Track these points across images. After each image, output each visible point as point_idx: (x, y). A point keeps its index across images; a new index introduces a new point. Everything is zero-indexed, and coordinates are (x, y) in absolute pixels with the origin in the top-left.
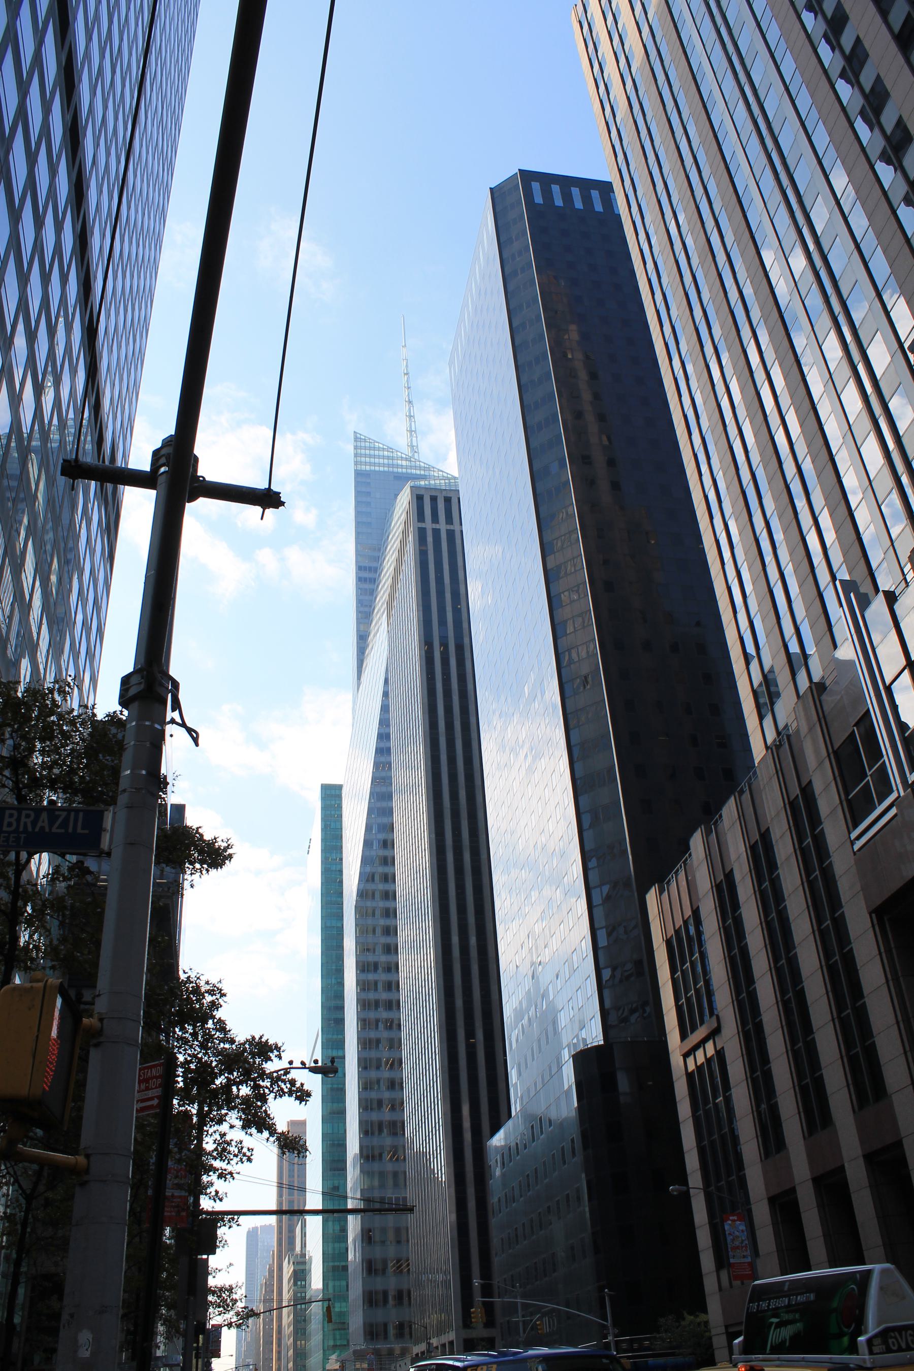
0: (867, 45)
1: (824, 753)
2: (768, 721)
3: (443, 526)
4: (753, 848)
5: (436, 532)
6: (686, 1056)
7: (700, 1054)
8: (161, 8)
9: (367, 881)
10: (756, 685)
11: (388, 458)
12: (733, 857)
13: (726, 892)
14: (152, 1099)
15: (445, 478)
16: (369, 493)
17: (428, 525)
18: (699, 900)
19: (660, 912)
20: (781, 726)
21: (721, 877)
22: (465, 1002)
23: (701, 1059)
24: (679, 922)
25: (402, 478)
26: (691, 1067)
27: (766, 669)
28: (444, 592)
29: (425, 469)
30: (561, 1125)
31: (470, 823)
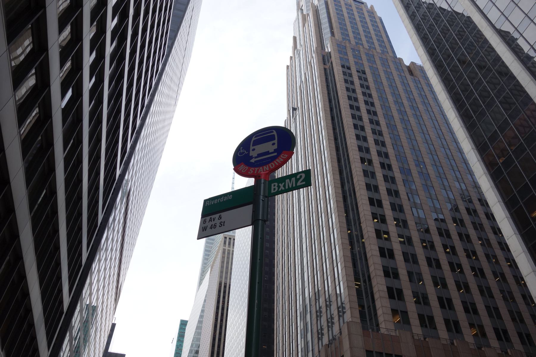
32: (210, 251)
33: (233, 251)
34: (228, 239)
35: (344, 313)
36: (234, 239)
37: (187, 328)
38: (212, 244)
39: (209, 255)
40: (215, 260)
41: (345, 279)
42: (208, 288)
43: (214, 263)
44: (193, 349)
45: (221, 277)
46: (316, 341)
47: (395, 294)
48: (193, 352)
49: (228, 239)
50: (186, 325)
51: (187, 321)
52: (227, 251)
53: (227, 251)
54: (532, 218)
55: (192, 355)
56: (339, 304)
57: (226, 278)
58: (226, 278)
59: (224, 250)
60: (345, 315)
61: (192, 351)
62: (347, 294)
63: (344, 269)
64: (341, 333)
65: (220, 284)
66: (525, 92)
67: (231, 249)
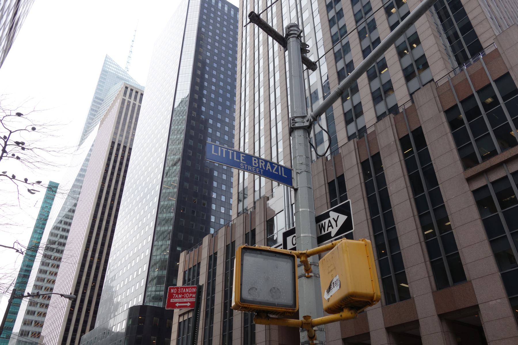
0: (351, 46)
1: (263, 220)
2: (241, 204)
3: (137, 103)
4: (227, 246)
5: (129, 102)
6: (180, 316)
7: (186, 317)
8: (190, 2)
9: (58, 223)
10: (240, 191)
11: (117, 69)
12: (219, 247)
13: (213, 259)
14: (187, 302)
15: (136, 84)
16: (105, 79)
17: (127, 98)
18: (201, 260)
19: (184, 261)
20: (245, 207)
21: (212, 253)
22: (86, 278)
23: (186, 317)
24: (191, 266)
25: (122, 79)
26: (181, 320)
27: (245, 187)
28: (125, 125)
29: (129, 78)
30: (118, 334)
31: (103, 209)
32: (96, 111)
33: (139, 107)
34: (129, 90)
35: (244, 198)
36: (142, 95)
38: (100, 104)
39: (95, 115)
40: (109, 111)
43: (106, 116)
44: (66, 206)
45: (115, 133)
48: (67, 210)
49: (129, 90)
52: (131, 104)
53: (131, 104)
54: (433, 229)
55: (65, 213)
56: (241, 189)
58: (127, 138)
59: (123, 101)
60: (245, 201)
61: (65, 209)
62: (418, 111)
64: (254, 207)
66: (461, 261)
67: (137, 103)
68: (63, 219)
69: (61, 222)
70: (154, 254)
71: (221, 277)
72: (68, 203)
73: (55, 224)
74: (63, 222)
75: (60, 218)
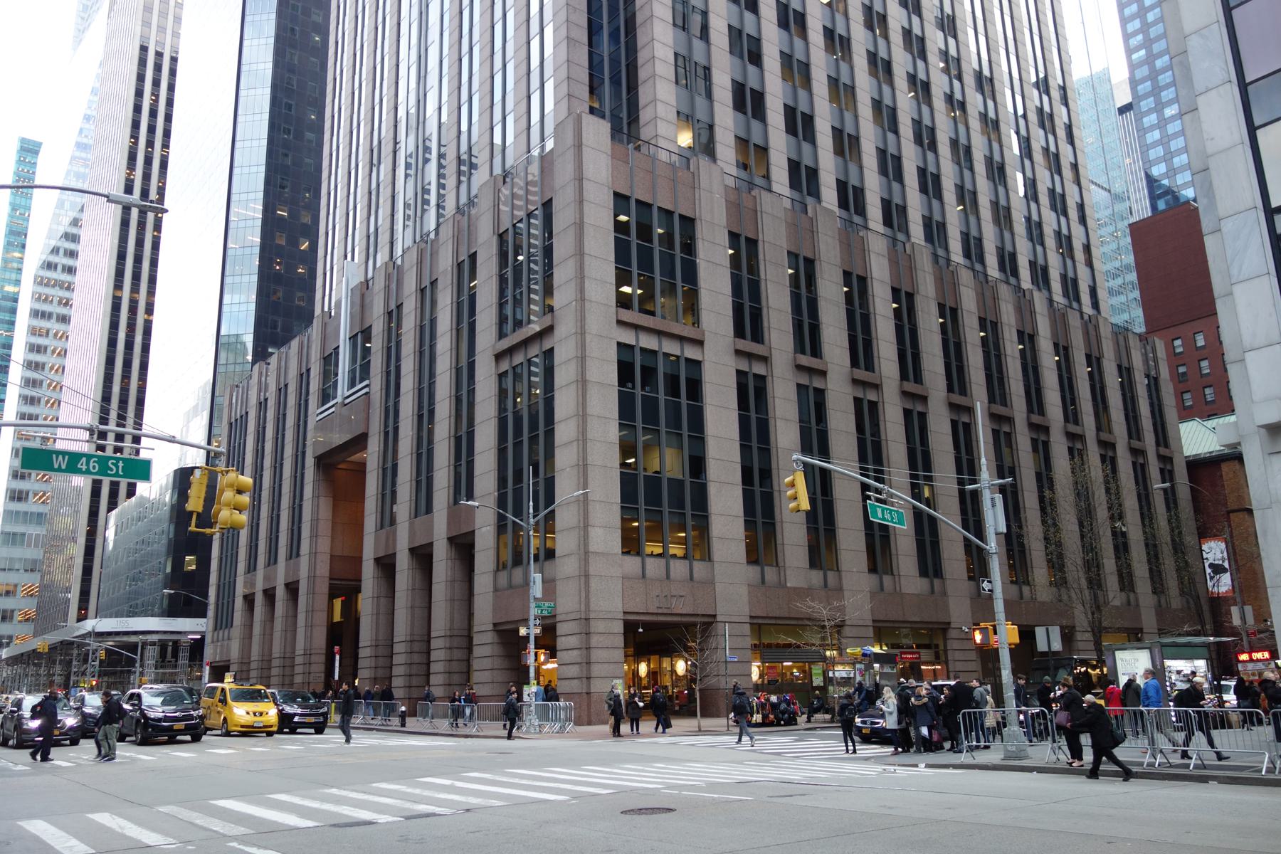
9: (52, 251)
37: (42, 160)
41: (563, 15)
42: (106, 53)
45: (146, 24)
46: (451, 182)
47: (692, 74)
50: (37, 153)
51: (40, 145)
57: (162, 29)
58: (162, 29)
63: (565, 43)
65: (144, 49)
68: (59, 244)
69: (55, 251)
70: (222, 360)
71: (411, 345)
72: (67, 205)
73: (44, 257)
74: (62, 252)
75: (53, 243)
